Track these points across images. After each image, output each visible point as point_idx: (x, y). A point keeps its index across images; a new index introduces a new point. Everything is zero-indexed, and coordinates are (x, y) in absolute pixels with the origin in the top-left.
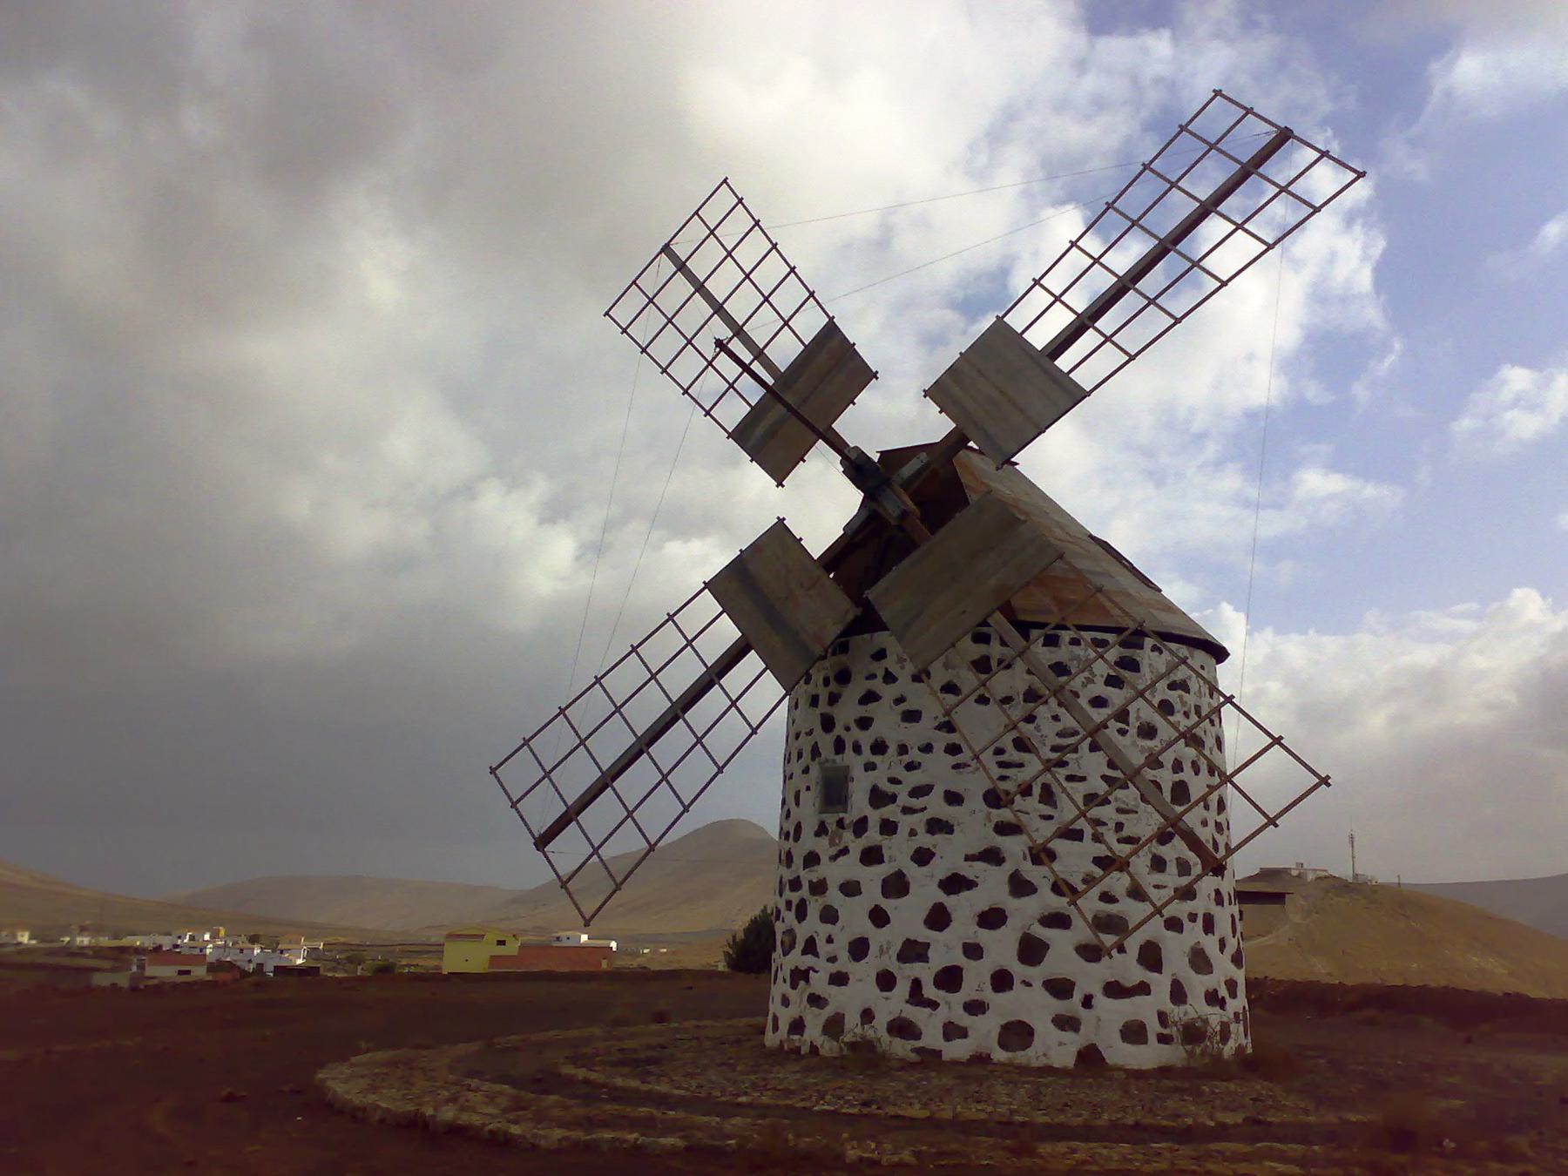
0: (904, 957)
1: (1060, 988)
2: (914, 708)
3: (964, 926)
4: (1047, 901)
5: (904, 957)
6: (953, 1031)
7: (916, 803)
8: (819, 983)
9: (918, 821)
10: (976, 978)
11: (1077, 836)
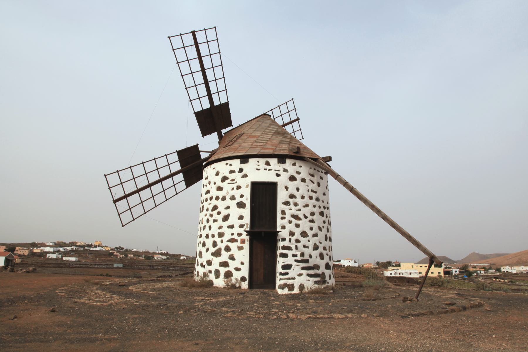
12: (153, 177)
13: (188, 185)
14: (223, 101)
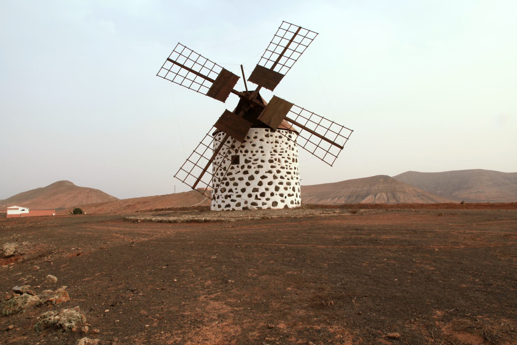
1: (281, 195)
6: (264, 204)
11: (283, 168)
13: (291, 105)
14: (282, 72)
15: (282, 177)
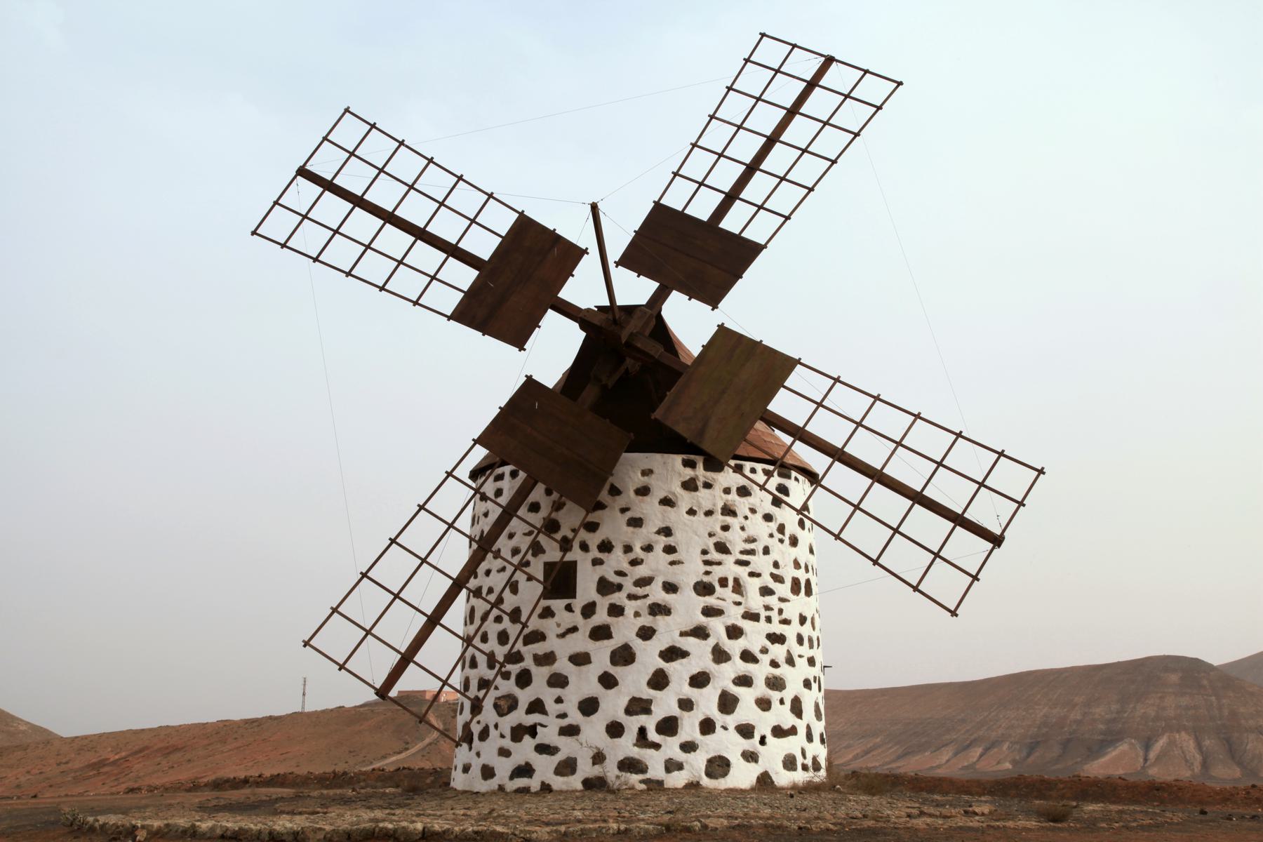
0: (629, 711)
1: (746, 731)
2: (638, 515)
3: (679, 686)
4: (737, 666)
5: (629, 711)
7: (639, 591)
8: (549, 735)
9: (642, 605)
10: (689, 728)
12: (384, 195)
13: (462, 315)
14: (754, 234)
15: (747, 656)
